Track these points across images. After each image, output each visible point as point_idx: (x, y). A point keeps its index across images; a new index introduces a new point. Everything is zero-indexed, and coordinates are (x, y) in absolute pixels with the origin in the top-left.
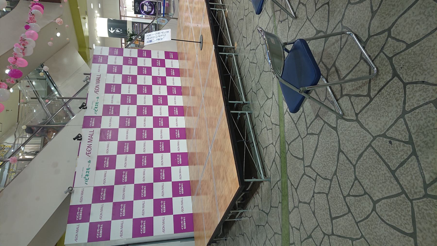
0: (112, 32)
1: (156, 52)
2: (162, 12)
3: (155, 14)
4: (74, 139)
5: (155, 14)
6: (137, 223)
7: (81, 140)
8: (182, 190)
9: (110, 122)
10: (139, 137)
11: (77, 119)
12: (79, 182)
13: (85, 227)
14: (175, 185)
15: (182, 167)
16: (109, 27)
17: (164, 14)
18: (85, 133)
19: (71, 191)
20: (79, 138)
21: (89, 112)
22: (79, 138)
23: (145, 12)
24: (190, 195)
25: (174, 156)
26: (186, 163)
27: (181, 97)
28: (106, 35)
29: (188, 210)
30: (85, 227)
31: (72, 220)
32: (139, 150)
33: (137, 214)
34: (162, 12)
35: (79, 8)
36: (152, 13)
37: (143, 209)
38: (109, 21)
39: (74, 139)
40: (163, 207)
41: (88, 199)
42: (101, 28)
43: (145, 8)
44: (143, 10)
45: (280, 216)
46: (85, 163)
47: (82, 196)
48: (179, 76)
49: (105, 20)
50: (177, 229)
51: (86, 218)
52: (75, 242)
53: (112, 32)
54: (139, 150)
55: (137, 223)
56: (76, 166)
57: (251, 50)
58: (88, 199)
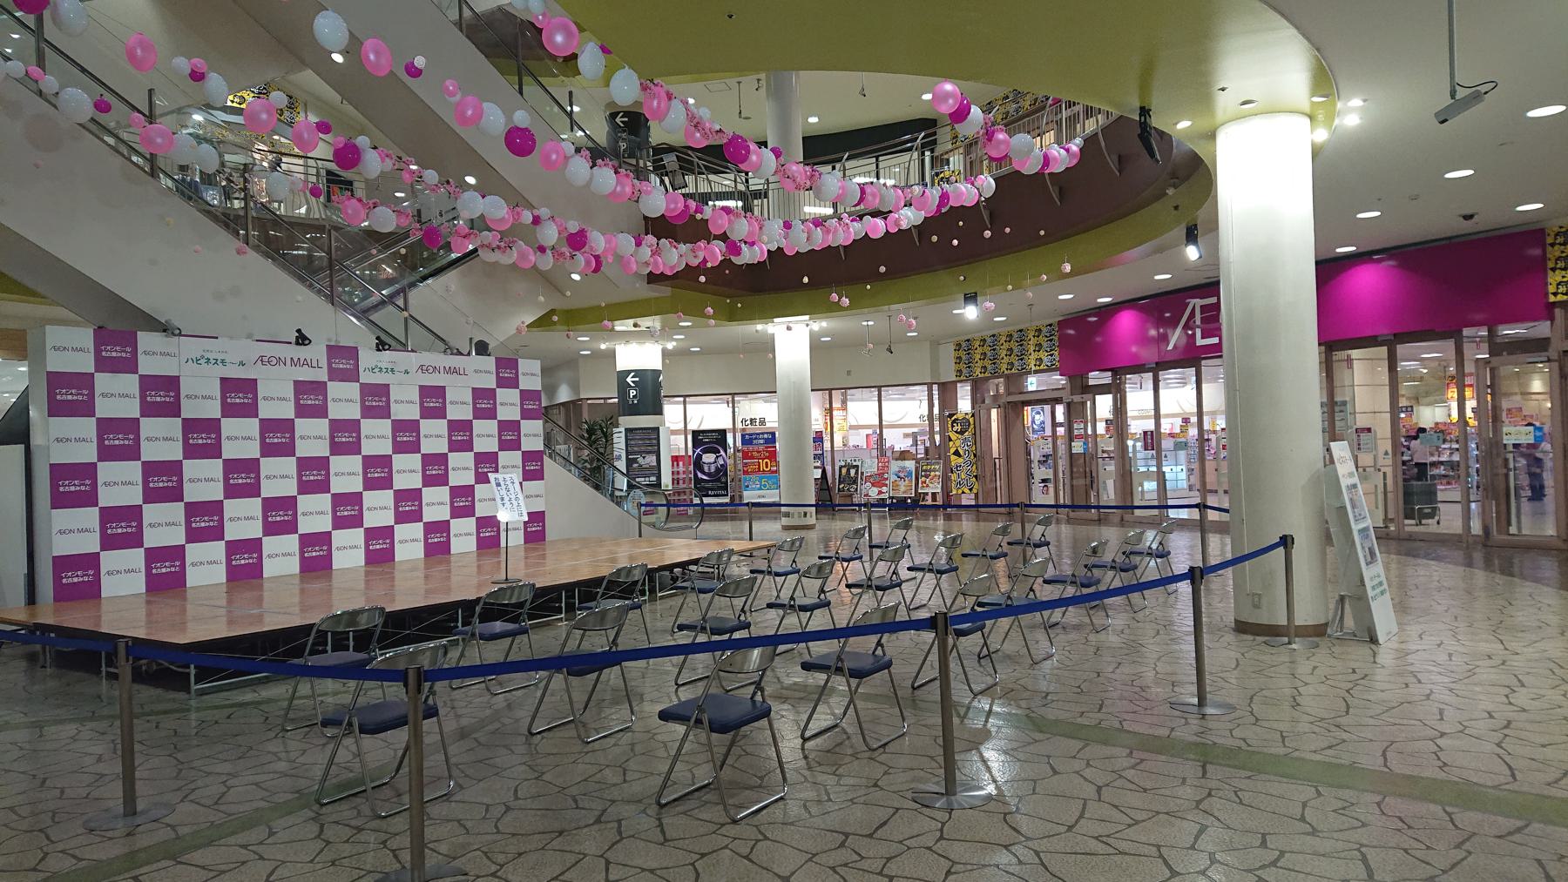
0: (629, 380)
1: (542, 492)
2: (706, 500)
3: (697, 480)
4: (299, 331)
5: (697, 480)
6: (87, 471)
7: (297, 343)
8: (377, 546)
9: (344, 401)
10: (505, 426)
11: (352, 331)
12: (191, 347)
13: (84, 363)
14: (324, 539)
15: (297, 559)
16: (638, 373)
17: (702, 504)
18: (317, 352)
19: (165, 329)
20: (302, 339)
21: (368, 358)
22: (302, 339)
23: (699, 457)
24: (148, 590)
25: (443, 527)
26: (234, 574)
27: (141, 587)
28: (621, 365)
29: (194, 578)
30: (84, 363)
31: (103, 336)
32: (480, 426)
33: (303, 426)
34: (706, 500)
35: (1170, 191)
36: (700, 475)
37: (120, 484)
38: (656, 373)
39: (299, 331)
40: (121, 527)
41: (147, 366)
42: (638, 354)
43: (708, 458)
44: (706, 451)
45: (155, 866)
46: (238, 357)
47: (154, 354)
48: (427, 555)
49: (656, 364)
50: (64, 564)
51: (103, 365)
52: (48, 346)
53: (629, 380)
54: (480, 426)
55: (87, 471)
56: (231, 338)
57: (1055, 772)
58: (147, 366)
